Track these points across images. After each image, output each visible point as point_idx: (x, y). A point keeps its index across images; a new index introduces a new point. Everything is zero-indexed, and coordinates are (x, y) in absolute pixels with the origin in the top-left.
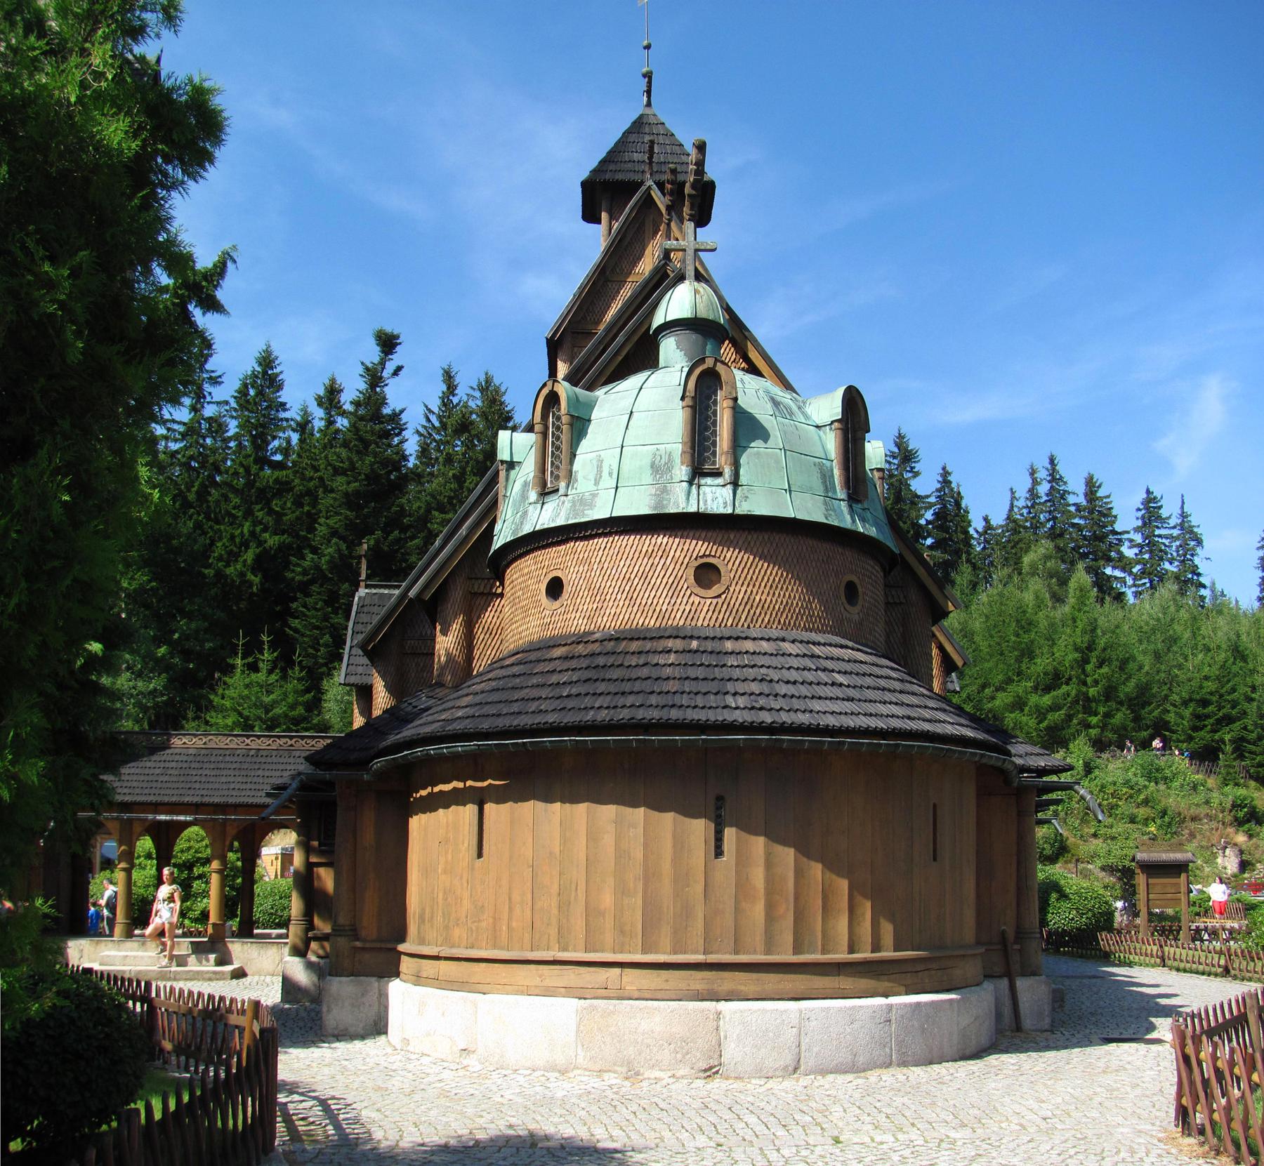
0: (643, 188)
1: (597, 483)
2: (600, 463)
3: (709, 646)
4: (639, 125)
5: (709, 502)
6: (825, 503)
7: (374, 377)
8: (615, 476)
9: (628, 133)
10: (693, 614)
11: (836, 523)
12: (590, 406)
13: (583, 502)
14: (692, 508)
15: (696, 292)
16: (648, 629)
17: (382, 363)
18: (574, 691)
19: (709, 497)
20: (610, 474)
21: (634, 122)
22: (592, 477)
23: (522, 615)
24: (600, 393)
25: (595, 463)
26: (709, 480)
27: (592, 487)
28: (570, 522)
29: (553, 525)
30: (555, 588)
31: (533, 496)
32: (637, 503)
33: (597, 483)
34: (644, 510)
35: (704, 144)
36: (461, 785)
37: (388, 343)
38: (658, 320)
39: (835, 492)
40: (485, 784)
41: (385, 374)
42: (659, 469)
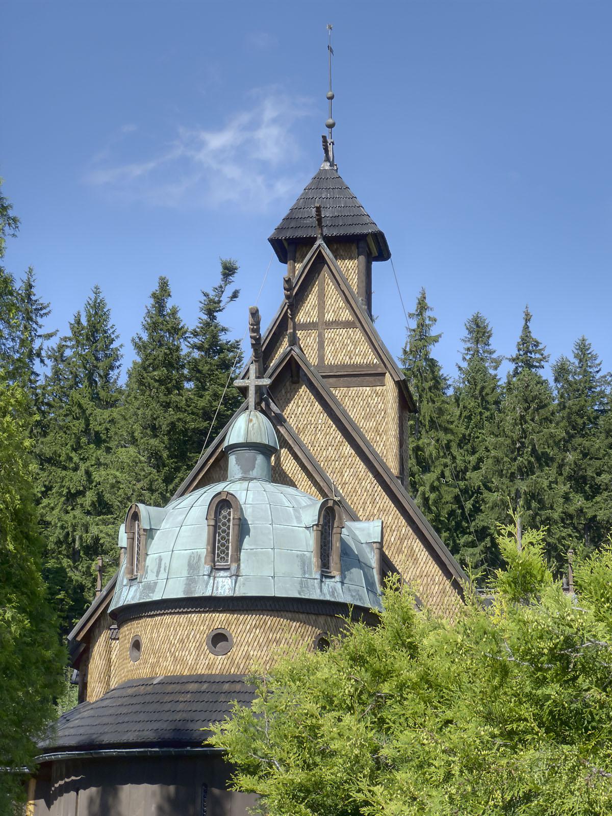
0: (315, 246)
1: (157, 576)
2: (160, 560)
3: (214, 688)
4: (320, 180)
5: (220, 588)
6: (301, 583)
7: (212, 308)
8: (167, 571)
10: (209, 667)
11: (307, 597)
13: (151, 588)
15: (250, 421)
16: (183, 676)
17: (220, 290)
18: (126, 719)
19: (220, 585)
20: (165, 570)
22: (155, 571)
23: (114, 665)
25: (158, 561)
26: (222, 573)
27: (154, 578)
28: (141, 601)
29: (133, 602)
30: (137, 645)
31: (125, 582)
32: (175, 591)
33: (157, 576)
34: (181, 595)
35: (257, 311)
36: (67, 780)
37: (229, 271)
39: (311, 574)
40: (70, 779)
41: (225, 298)
42: (192, 566)
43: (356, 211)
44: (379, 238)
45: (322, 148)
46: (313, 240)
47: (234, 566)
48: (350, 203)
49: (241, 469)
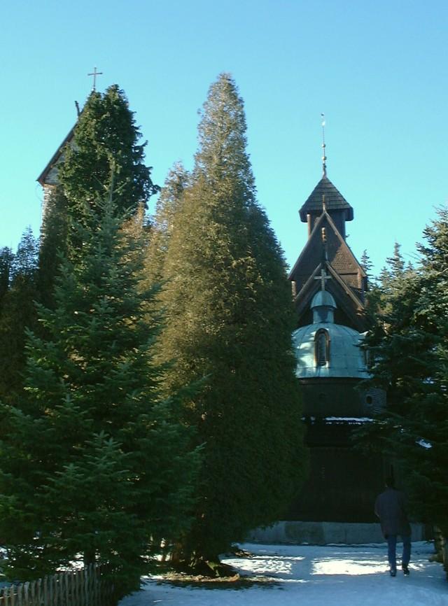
0: (323, 215)
21: (319, 183)
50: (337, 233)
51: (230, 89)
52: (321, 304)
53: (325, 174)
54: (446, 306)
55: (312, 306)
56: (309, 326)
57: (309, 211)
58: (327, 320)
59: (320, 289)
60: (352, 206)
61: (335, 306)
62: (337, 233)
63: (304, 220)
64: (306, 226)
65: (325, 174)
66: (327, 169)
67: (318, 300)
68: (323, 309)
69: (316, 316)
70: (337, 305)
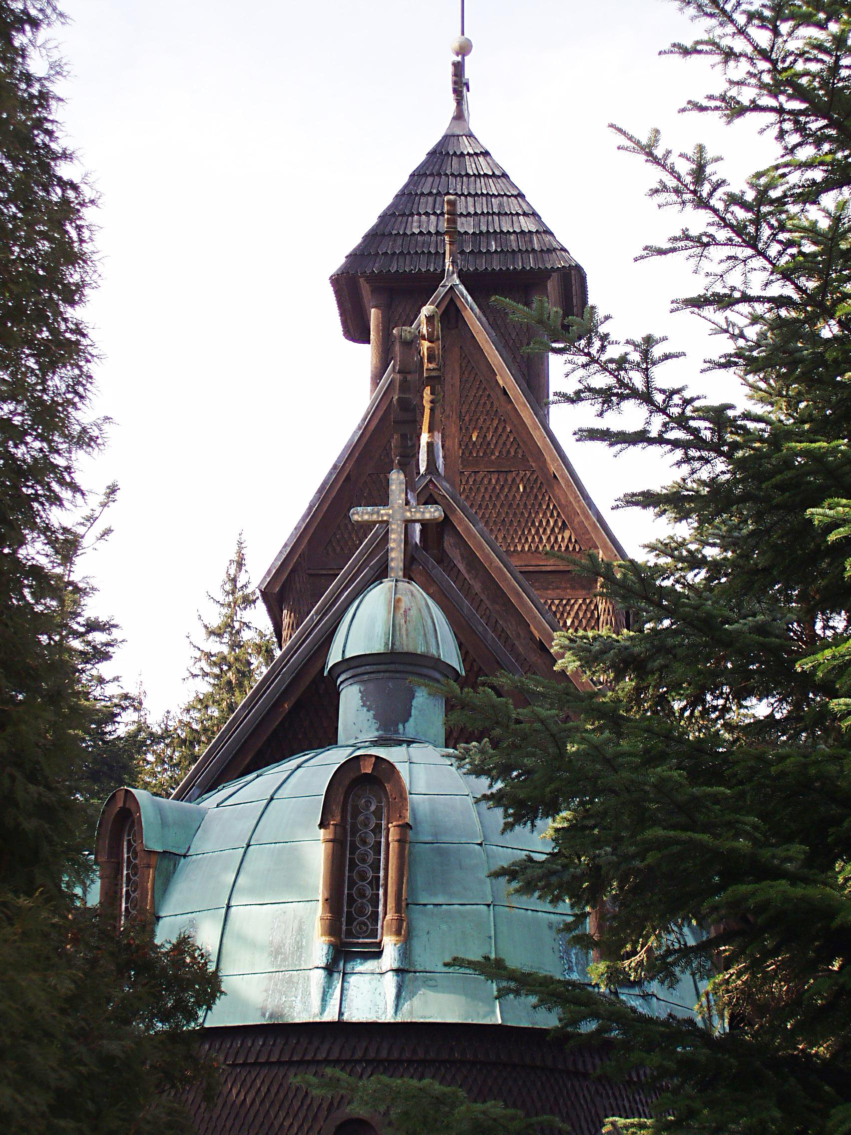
0: (441, 291)
9: (418, 176)
12: (192, 826)
14: (330, 1015)
21: (432, 154)
24: (210, 801)
38: (334, 657)
43: (527, 225)
44: (573, 281)
45: (450, 87)
46: (440, 276)
47: (390, 945)
48: (514, 206)
49: (375, 717)
50: (506, 378)
51: (503, 833)
52: (378, 647)
53: (460, 116)
54: (847, 87)
55: (334, 657)
56: (422, 1020)
57: (378, 284)
58: (410, 728)
59: (381, 573)
60: (579, 254)
61: (450, 654)
62: (506, 378)
63: (356, 330)
64: (364, 356)
65: (460, 116)
66: (470, 97)
67: (367, 624)
68: (394, 670)
69: (350, 698)
70: (465, 656)
